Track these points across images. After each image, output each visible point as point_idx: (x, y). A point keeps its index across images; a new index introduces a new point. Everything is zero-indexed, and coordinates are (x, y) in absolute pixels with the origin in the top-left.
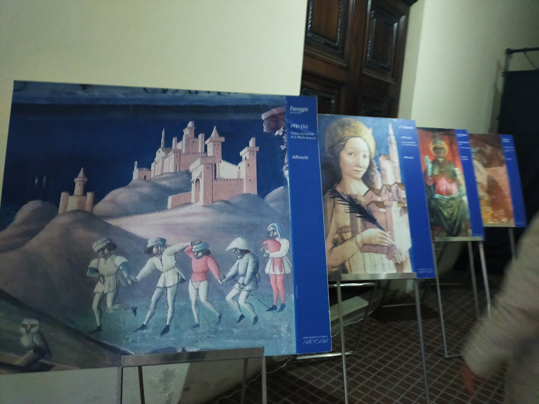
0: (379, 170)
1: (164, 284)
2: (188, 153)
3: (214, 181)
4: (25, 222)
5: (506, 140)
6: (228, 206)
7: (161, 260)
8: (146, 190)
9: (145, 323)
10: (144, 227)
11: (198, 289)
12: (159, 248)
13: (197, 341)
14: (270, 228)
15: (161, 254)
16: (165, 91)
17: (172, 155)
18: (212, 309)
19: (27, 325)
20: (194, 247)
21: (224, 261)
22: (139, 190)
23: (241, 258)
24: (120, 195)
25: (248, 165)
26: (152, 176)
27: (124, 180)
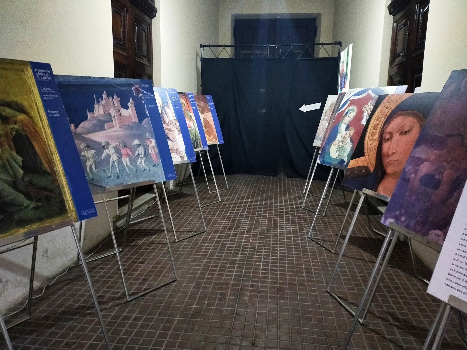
0: (166, 113)
2: (107, 105)
5: (209, 98)
6: (128, 127)
8: (95, 122)
10: (99, 137)
11: (126, 161)
15: (108, 148)
16: (90, 77)
18: (134, 168)
21: (133, 149)
22: (92, 122)
24: (84, 125)
27: (85, 118)
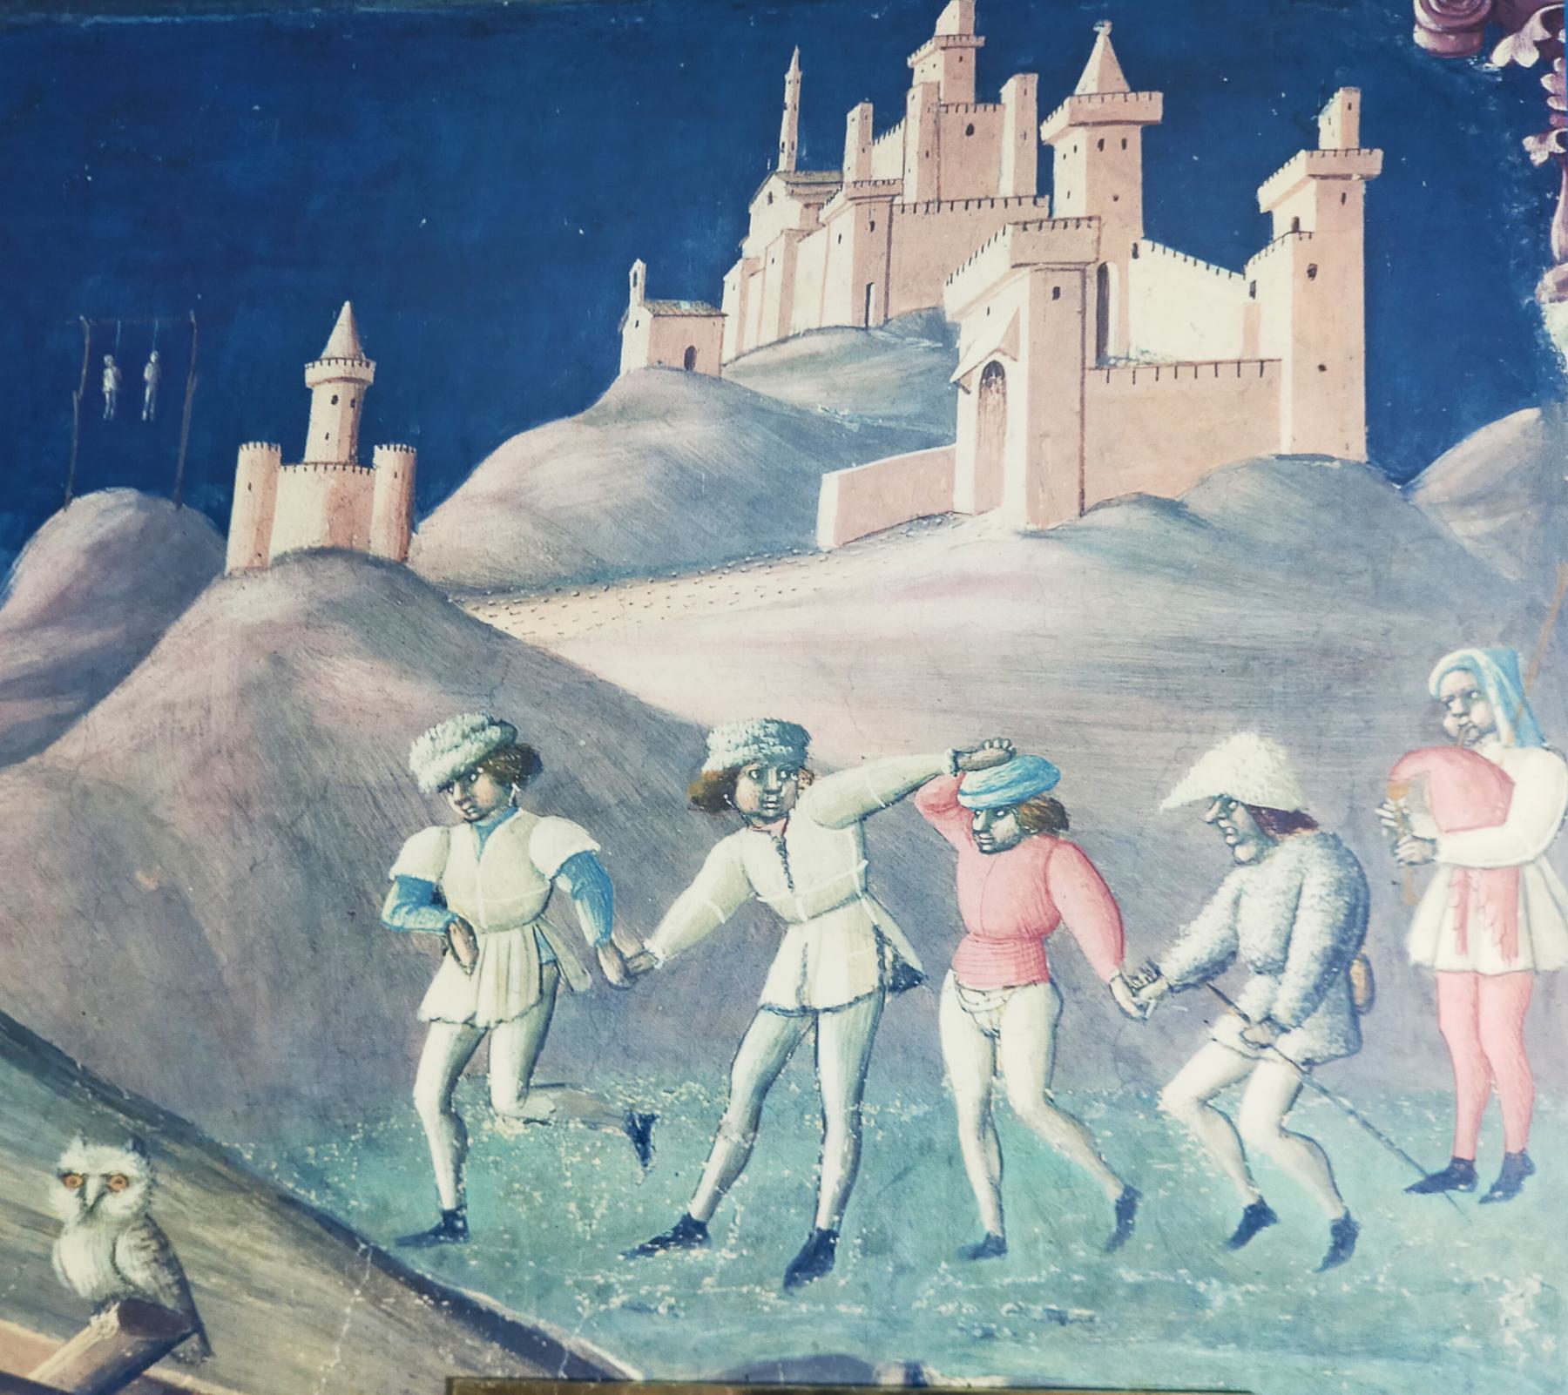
1: (799, 991)
3: (1095, 379)
4: (61, 610)
7: (782, 849)
8: (695, 434)
9: (696, 1209)
12: (773, 784)
13: (988, 1335)
14: (1445, 679)
15: (783, 815)
17: (842, 216)
19: (85, 1177)
20: (972, 781)
23: (1255, 860)
24: (543, 469)
25: (1312, 272)
26: (728, 354)
27: (574, 378)
